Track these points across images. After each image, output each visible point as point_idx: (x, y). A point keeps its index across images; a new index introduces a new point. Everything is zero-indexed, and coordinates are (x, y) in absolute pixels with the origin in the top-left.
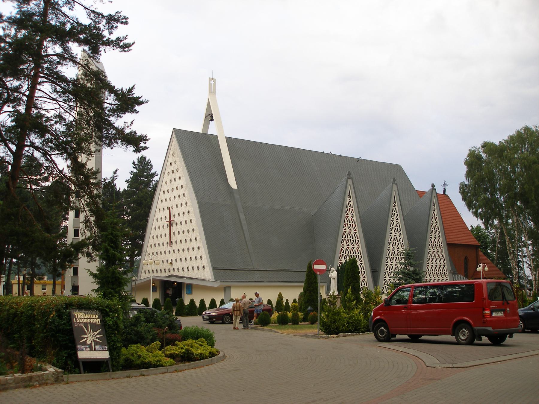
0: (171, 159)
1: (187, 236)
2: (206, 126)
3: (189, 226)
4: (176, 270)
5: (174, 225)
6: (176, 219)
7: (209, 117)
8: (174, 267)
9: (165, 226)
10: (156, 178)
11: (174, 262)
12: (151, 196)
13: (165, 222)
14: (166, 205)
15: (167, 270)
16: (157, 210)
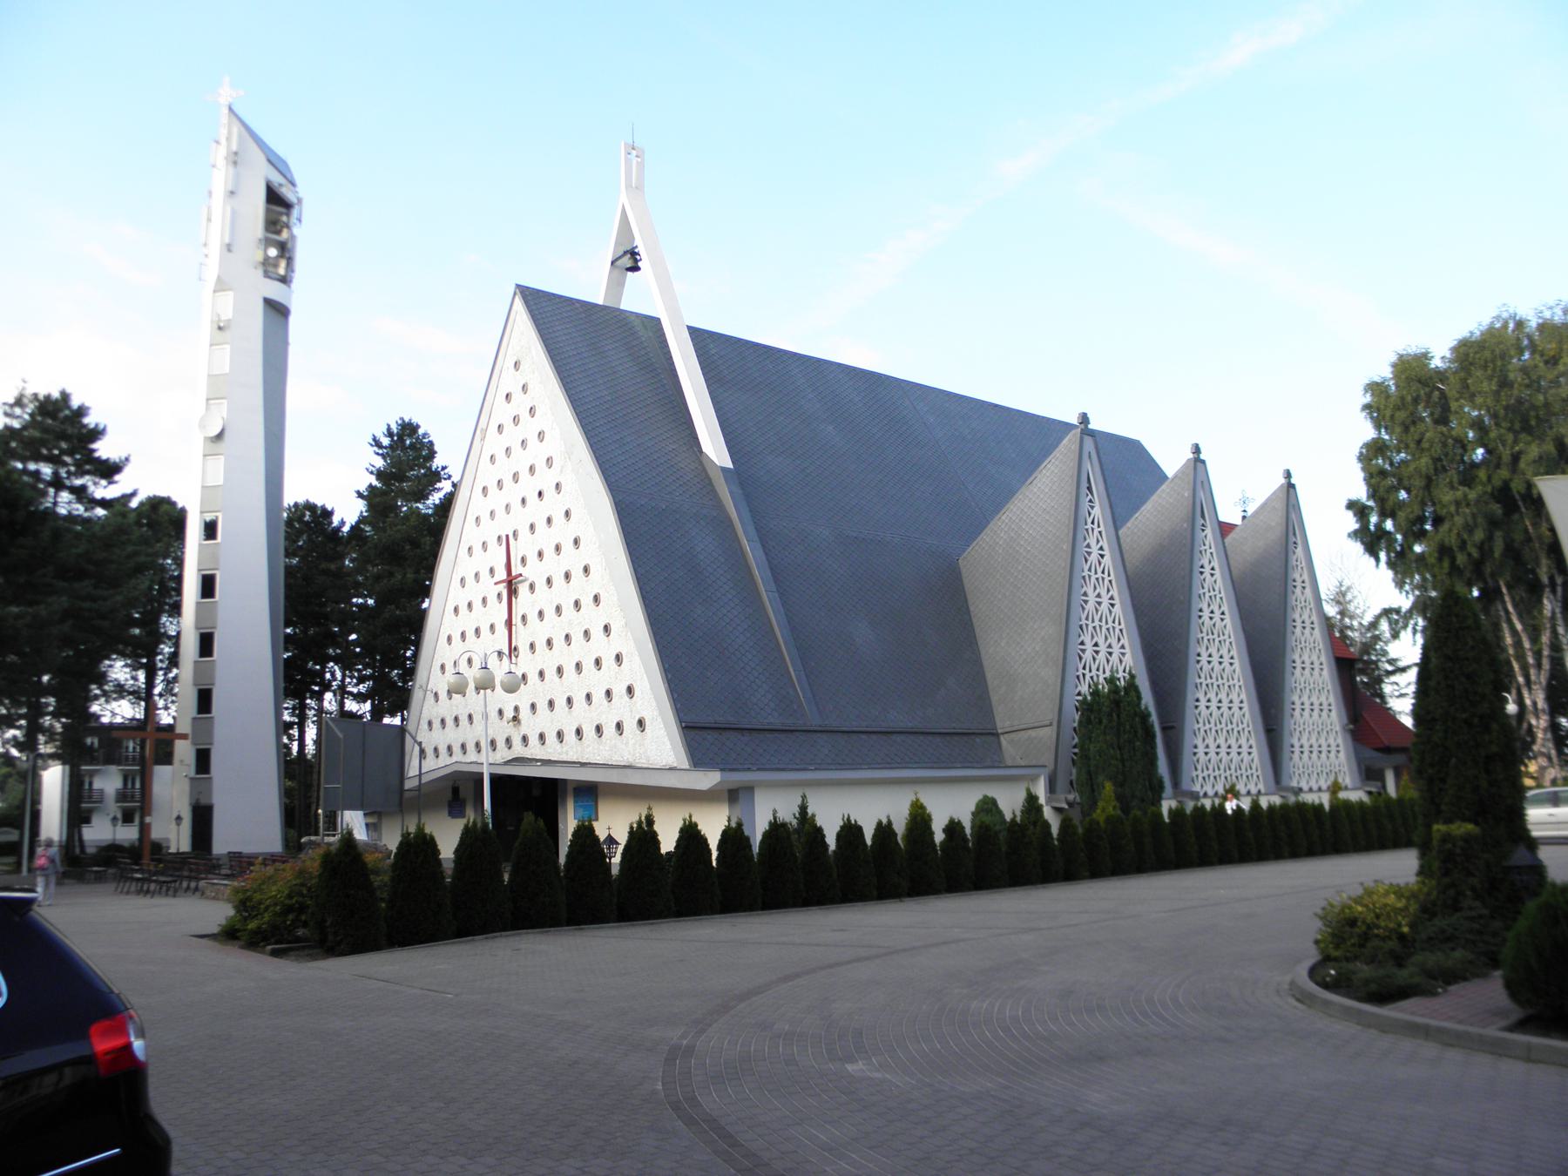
0: (509, 381)
1: (573, 622)
2: (616, 286)
3: (582, 588)
4: (534, 740)
5: (523, 589)
6: (532, 572)
7: (630, 260)
8: (524, 729)
9: (492, 599)
10: (446, 486)
11: (525, 713)
12: (435, 527)
13: (493, 588)
14: (490, 530)
15: (501, 744)
16: (463, 551)
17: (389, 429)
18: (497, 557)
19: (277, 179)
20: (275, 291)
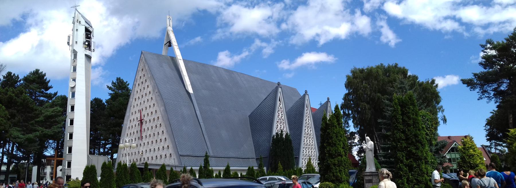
6: (146, 119)
13: (137, 123)
14: (137, 109)
16: (131, 114)
17: (108, 87)
18: (138, 115)
19: (87, 26)
20: (88, 52)
